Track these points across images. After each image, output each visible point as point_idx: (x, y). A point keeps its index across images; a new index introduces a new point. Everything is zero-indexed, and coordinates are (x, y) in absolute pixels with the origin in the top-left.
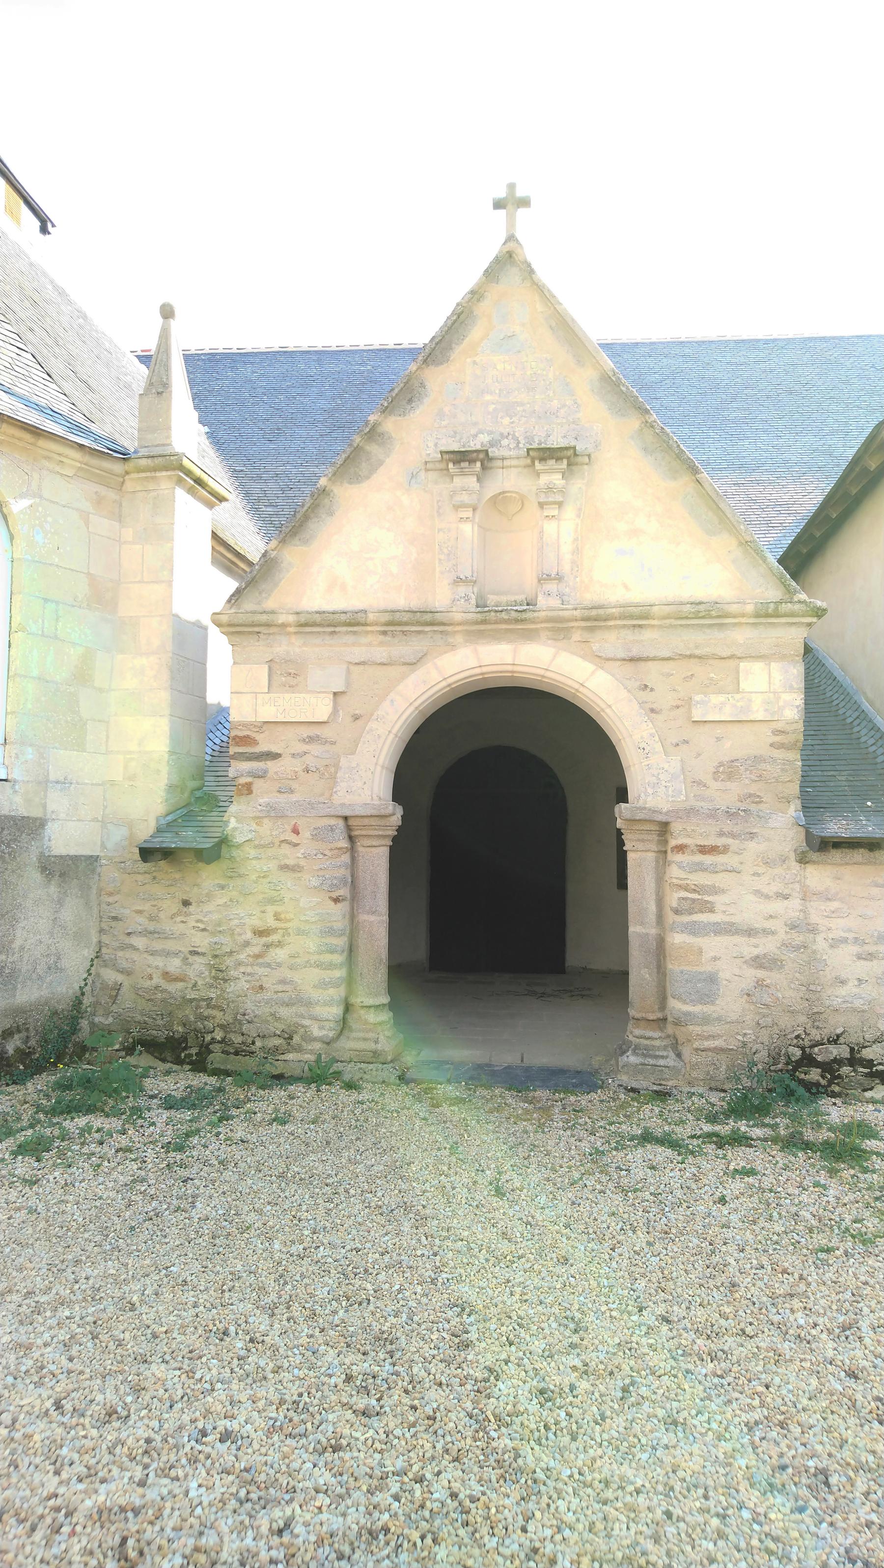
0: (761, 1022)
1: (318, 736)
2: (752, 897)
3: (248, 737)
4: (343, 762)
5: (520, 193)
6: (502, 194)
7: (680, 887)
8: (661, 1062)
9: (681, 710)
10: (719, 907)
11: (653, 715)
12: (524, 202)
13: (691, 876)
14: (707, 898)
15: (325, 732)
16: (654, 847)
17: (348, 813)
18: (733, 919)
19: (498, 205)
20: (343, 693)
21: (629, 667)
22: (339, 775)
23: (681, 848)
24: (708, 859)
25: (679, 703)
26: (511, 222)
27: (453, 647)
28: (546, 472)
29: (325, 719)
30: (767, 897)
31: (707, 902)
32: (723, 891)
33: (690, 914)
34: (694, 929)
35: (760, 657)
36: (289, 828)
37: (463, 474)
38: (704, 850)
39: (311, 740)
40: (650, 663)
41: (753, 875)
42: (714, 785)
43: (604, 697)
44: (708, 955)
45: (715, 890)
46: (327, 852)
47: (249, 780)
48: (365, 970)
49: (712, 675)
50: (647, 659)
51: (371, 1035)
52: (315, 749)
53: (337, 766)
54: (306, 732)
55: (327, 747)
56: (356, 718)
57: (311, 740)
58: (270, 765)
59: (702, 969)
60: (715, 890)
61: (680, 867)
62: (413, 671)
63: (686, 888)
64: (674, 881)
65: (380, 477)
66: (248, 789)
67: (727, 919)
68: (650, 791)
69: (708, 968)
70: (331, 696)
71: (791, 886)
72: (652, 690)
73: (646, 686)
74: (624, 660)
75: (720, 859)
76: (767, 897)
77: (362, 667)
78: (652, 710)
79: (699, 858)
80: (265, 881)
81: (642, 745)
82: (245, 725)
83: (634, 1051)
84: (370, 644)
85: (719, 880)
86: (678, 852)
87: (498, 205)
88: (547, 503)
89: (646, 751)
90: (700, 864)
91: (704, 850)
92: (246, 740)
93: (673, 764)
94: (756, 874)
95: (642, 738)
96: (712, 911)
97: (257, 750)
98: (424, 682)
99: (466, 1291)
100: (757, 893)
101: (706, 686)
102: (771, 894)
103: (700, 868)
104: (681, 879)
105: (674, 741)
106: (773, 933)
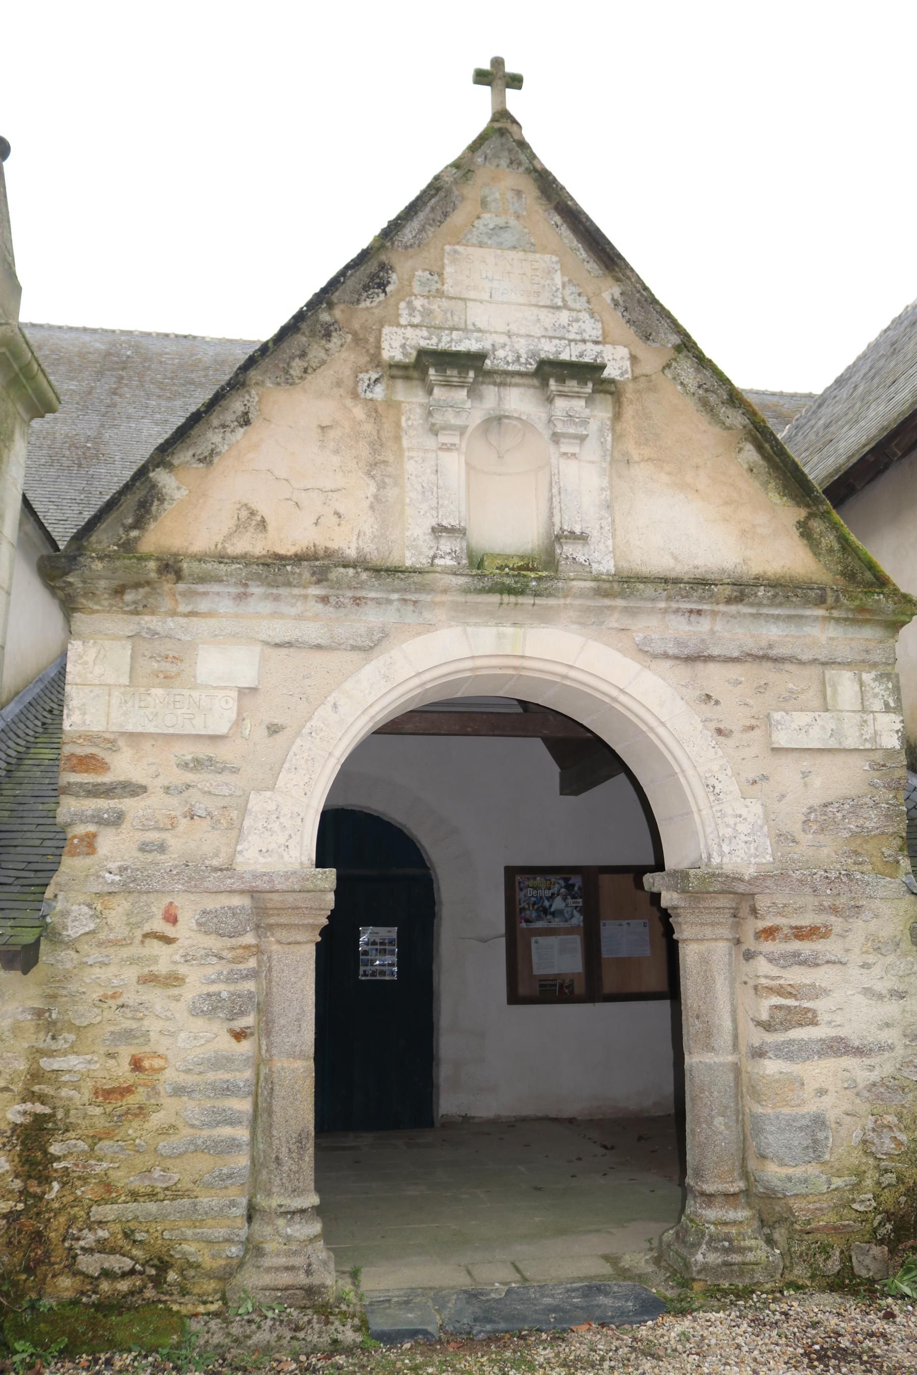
0: (882, 1179)
1: (210, 759)
2: (860, 999)
3: (93, 757)
4: (256, 802)
5: (509, 68)
6: (487, 66)
7: (770, 989)
8: (750, 1257)
9: (757, 733)
10: (823, 1017)
11: (721, 739)
12: (516, 82)
13: (785, 973)
14: (806, 1004)
15: (223, 753)
16: (726, 932)
17: (260, 884)
18: (842, 1032)
19: (481, 77)
20: (253, 690)
21: (683, 672)
22: (246, 824)
23: (770, 933)
24: (805, 947)
25: (754, 722)
26: (499, 98)
27: (430, 627)
28: (562, 395)
29: (223, 730)
30: (881, 997)
31: (808, 1010)
32: (826, 992)
33: (787, 1029)
34: (788, 1052)
35: (849, 664)
36: (158, 910)
37: (448, 385)
38: (800, 933)
39: (198, 764)
40: (712, 666)
41: (862, 967)
42: (806, 839)
43: (656, 710)
44: (811, 1087)
45: (817, 992)
46: (225, 954)
47: (92, 828)
48: (284, 1150)
49: (791, 685)
50: (710, 658)
51: (299, 1261)
52: (205, 779)
53: (244, 811)
54: (188, 752)
55: (226, 777)
56: (274, 730)
57: (198, 764)
58: (127, 804)
59: (804, 1110)
60: (817, 992)
61: (770, 961)
62: (368, 661)
63: (780, 991)
64: (763, 981)
65: (321, 380)
66: (89, 843)
67: (833, 1033)
68: (726, 849)
69: (812, 1107)
70: (235, 694)
71: (907, 979)
72: (717, 702)
73: (708, 697)
74: (676, 658)
75: (819, 946)
76: (881, 997)
77: (284, 651)
78: (719, 731)
79: (796, 945)
80: (113, 1003)
81: (712, 781)
82: (91, 738)
83: (709, 1243)
84: (299, 617)
85: (821, 976)
86: (766, 939)
87: (481, 77)
88: (564, 435)
89: (717, 790)
90: (796, 954)
91: (800, 933)
92: (88, 763)
93: (753, 810)
94: (866, 966)
95: (710, 771)
96: (814, 1023)
97: (107, 778)
98: (386, 678)
99: (213, 441)
100: (868, 992)
101: (785, 700)
102: (884, 992)
103: (798, 960)
104: (773, 978)
105: (751, 776)
106: (891, 1048)
